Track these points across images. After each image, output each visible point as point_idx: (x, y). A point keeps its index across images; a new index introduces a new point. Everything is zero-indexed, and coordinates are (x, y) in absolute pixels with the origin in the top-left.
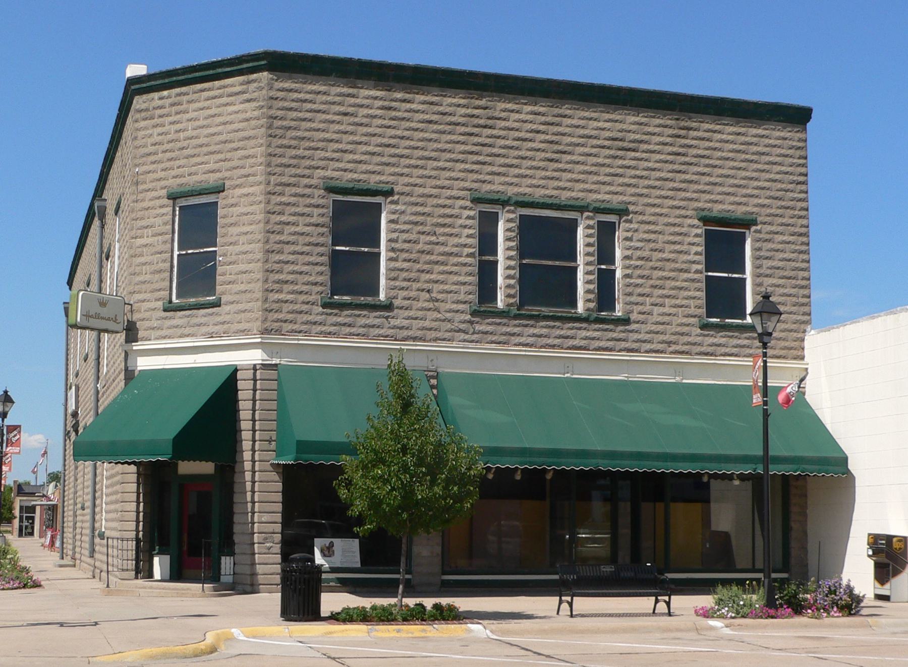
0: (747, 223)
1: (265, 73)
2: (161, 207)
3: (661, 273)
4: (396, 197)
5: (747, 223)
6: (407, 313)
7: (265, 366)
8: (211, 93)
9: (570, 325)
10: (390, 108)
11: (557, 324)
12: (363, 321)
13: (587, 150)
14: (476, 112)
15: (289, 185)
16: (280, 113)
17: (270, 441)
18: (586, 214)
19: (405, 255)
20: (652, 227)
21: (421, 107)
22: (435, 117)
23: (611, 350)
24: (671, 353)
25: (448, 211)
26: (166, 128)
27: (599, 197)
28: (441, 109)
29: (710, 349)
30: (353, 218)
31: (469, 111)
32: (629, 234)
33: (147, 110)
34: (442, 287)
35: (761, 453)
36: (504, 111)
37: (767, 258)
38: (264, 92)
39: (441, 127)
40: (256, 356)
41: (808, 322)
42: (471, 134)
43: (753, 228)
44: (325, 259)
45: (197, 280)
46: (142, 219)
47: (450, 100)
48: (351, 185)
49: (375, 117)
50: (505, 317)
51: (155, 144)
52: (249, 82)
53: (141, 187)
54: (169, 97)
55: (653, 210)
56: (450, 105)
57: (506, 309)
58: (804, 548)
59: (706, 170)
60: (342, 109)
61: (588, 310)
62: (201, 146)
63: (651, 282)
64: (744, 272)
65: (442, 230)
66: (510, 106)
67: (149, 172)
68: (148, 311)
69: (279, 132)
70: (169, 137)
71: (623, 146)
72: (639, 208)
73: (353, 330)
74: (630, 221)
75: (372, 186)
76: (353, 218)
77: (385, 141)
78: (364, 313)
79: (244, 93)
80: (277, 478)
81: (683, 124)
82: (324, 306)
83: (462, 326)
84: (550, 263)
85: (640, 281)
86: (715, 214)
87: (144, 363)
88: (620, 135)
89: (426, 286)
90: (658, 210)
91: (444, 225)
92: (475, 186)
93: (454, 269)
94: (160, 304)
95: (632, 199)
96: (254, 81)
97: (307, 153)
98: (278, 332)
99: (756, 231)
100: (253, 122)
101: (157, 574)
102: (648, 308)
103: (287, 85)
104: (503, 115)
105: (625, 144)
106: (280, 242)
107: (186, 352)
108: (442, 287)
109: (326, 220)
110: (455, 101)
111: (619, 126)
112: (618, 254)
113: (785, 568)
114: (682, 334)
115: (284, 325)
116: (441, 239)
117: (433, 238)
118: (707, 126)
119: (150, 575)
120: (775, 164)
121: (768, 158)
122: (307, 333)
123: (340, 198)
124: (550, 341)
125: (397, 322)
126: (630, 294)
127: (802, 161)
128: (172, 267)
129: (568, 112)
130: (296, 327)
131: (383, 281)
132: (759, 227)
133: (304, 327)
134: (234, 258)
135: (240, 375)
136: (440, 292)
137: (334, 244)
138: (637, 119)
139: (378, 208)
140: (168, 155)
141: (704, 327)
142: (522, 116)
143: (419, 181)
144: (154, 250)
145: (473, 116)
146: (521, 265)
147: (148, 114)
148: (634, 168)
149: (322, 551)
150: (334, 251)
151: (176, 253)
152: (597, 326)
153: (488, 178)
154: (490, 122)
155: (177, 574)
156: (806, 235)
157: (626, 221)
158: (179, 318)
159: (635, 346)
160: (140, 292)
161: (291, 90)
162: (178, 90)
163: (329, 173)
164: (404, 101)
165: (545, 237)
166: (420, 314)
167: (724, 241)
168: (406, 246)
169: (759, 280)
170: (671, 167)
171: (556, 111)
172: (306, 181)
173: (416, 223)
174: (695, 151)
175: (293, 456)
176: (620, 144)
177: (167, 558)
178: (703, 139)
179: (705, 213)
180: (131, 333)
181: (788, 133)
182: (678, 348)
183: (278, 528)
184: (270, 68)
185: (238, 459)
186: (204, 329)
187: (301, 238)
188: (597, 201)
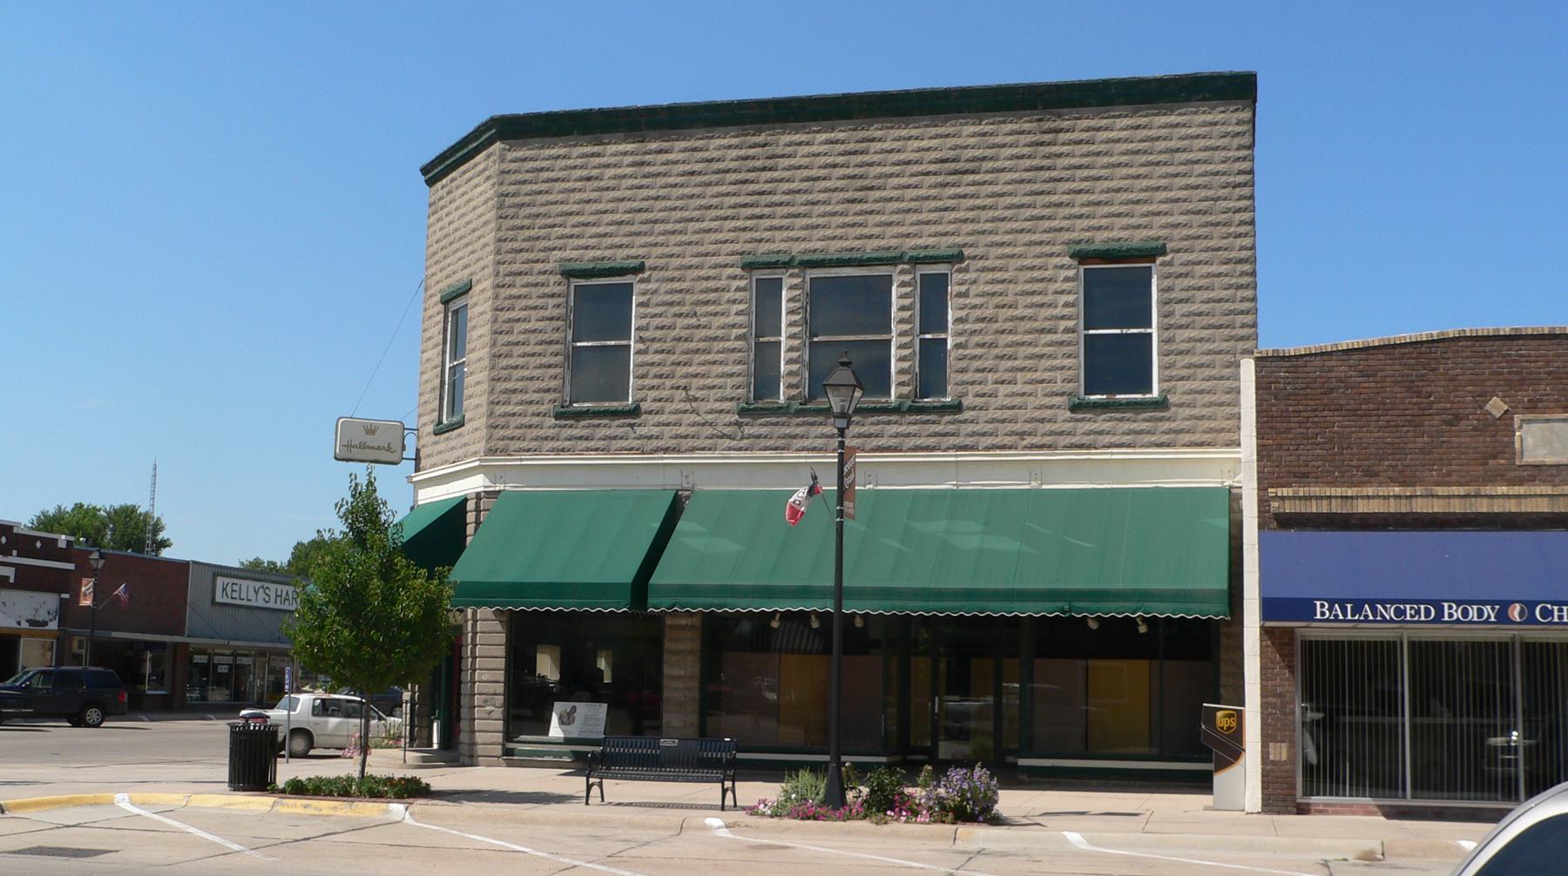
12: (603, 432)
35: (831, 583)
43: (1159, 260)
71: (956, 168)
94: (430, 428)
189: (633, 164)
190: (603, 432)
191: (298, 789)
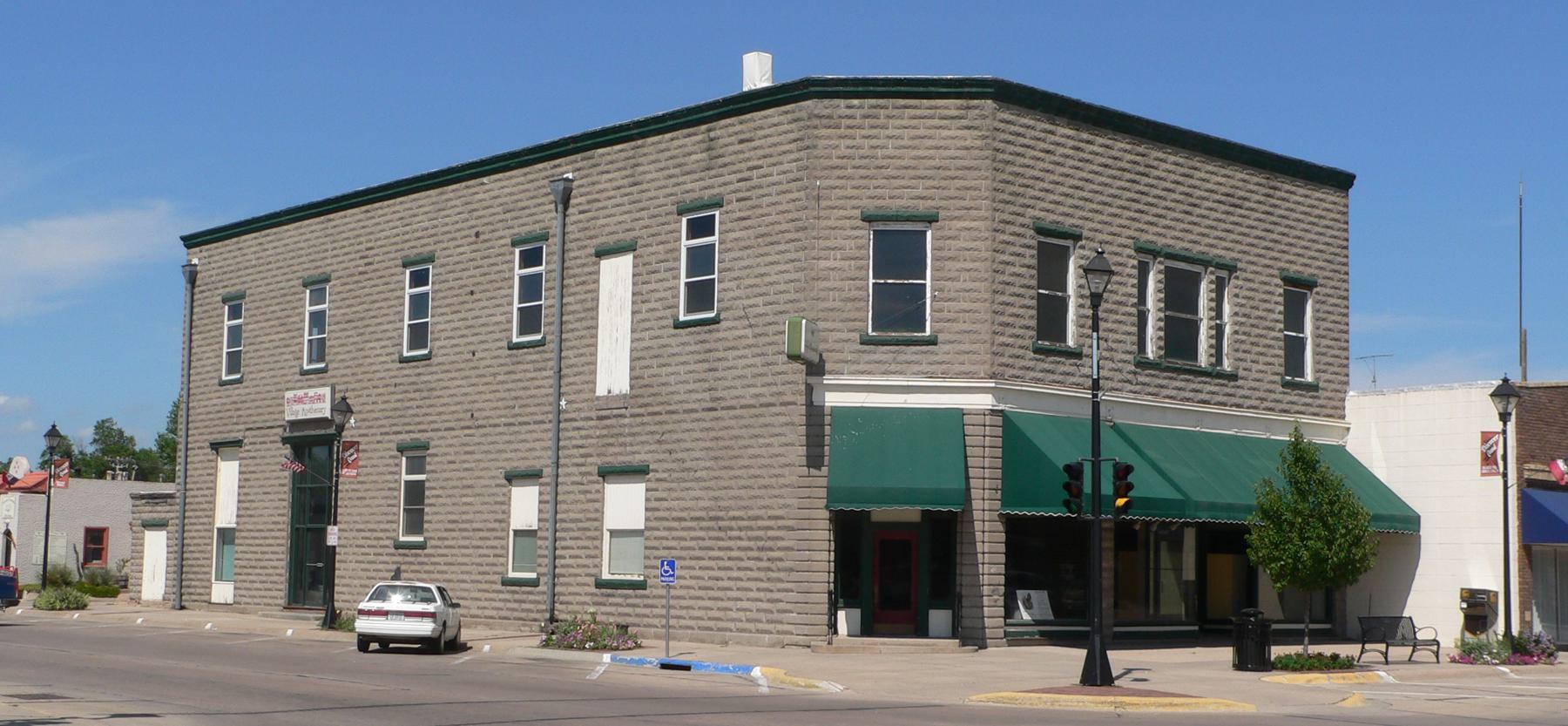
2: (853, 228)
7: (993, 412)
8: (918, 112)
10: (1078, 149)
12: (1062, 369)
16: (1001, 146)
22: (1110, 162)
26: (858, 141)
31: (1133, 157)
38: (988, 121)
40: (985, 401)
44: (1034, 303)
45: (899, 316)
46: (827, 238)
48: (1053, 227)
52: (968, 108)
53: (824, 203)
66: (1160, 155)
68: (839, 339)
70: (862, 152)
71: (1235, 203)
75: (1066, 229)
81: (1272, 183)
83: (1130, 377)
87: (832, 399)
88: (1231, 191)
92: (1136, 234)
94: (856, 336)
95: (1239, 256)
96: (976, 107)
98: (1002, 376)
134: (953, 295)
140: (862, 172)
147: (832, 122)
154: (1147, 170)
155: (868, 628)
158: (882, 353)
160: (825, 320)
162: (873, 101)
163: (1037, 213)
164: (1088, 142)
177: (857, 613)
180: (816, 369)
181: (1330, 197)
186: (916, 368)
189: (1074, 148)
190: (1062, 369)
191: (1286, 665)
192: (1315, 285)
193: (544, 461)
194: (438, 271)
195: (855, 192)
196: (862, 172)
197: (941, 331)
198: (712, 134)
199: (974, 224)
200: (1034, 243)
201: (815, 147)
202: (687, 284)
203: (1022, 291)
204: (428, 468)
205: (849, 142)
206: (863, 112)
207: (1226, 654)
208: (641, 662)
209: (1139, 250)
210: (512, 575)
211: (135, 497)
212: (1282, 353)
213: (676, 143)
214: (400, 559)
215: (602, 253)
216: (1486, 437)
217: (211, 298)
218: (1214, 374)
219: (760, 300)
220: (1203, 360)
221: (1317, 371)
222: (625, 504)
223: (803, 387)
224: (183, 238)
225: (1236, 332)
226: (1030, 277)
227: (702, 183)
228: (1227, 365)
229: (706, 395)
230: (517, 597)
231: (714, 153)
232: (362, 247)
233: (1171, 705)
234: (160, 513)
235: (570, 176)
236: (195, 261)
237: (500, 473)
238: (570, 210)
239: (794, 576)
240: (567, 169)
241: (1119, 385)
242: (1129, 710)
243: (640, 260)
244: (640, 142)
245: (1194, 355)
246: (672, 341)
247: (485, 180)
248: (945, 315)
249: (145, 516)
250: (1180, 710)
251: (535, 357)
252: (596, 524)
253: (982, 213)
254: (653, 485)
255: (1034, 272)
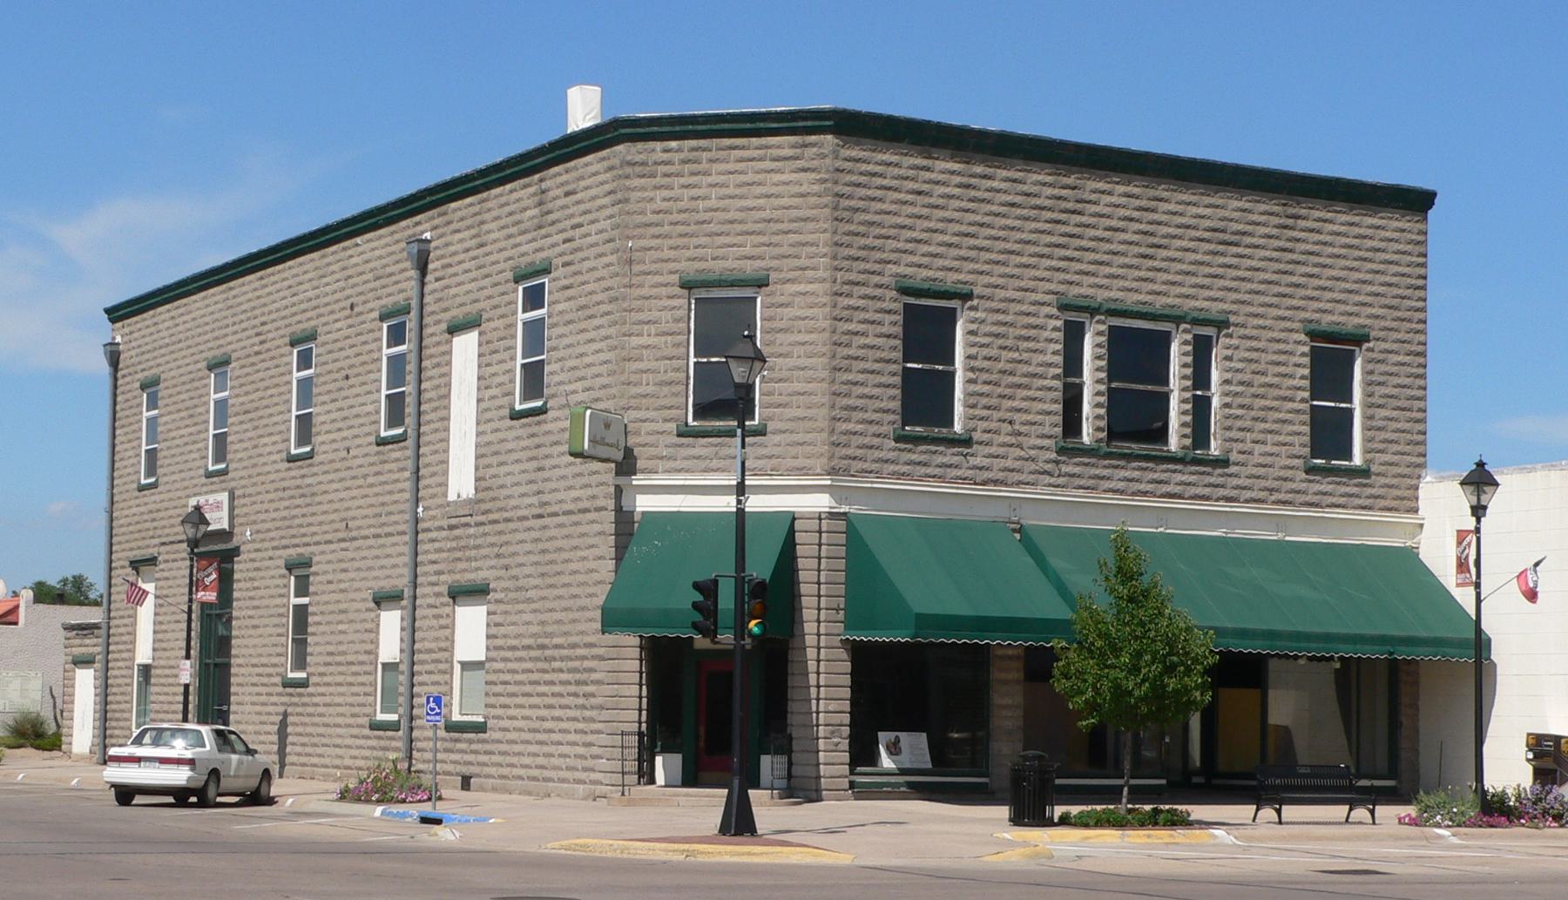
0: (1359, 339)
1: (829, 137)
2: (670, 297)
3: (1263, 402)
4: (975, 302)
5: (1359, 339)
6: (988, 450)
7: (832, 516)
9: (1164, 467)
10: (968, 186)
11: (1150, 465)
12: (940, 459)
13: (1185, 244)
14: (1064, 192)
15: (857, 284)
16: (847, 190)
17: (837, 610)
18: (1183, 326)
19: (985, 376)
20: (1254, 344)
21: (1003, 185)
22: (1018, 199)
23: (1208, 499)
24: (1274, 503)
25: (1032, 320)
26: (677, 192)
27: (1197, 304)
28: (1025, 188)
29: (1316, 499)
30: (926, 327)
31: (1056, 192)
32: (1229, 352)
33: (644, 164)
34: (1025, 417)
36: (1094, 191)
37: (1379, 384)
38: (827, 161)
39: (1025, 212)
40: (821, 502)
41: (1422, 466)
42: (1058, 222)
43: (1366, 346)
44: (897, 380)
45: (725, 404)
46: (640, 310)
47: (1035, 177)
48: (926, 286)
49: (952, 197)
50: (1093, 456)
51: (659, 212)
53: (637, 268)
54: (679, 150)
55: (1256, 322)
56: (1035, 183)
57: (1095, 445)
58: (1415, 751)
59: (1316, 270)
60: (916, 186)
61: (1184, 448)
62: (731, 222)
63: (1253, 413)
64: (1350, 401)
65: (1026, 344)
66: (1101, 185)
67: (650, 249)
69: (846, 214)
70: (681, 205)
71: (1225, 239)
72: (1240, 319)
73: (929, 471)
74: (1230, 336)
76: (926, 327)
77: (964, 228)
78: (941, 448)
79: (797, 158)
80: (845, 656)
81: (1291, 211)
82: (897, 440)
83: (1048, 467)
84: (1141, 387)
85: (1240, 412)
86: (1324, 327)
87: (645, 504)
88: (1221, 225)
89: (1008, 415)
90: (1261, 322)
91: (1028, 339)
92: (1062, 288)
93: (1039, 394)
94: (672, 426)
95: (1234, 307)
97: (878, 242)
98: (846, 472)
99: (1369, 350)
100: (813, 200)
101: (660, 776)
102: (1248, 446)
103: (854, 153)
104: (1093, 197)
105: (1226, 237)
106: (848, 357)
107: (685, 490)
108: (1025, 417)
109: (898, 330)
110: (1040, 178)
111: (1221, 213)
112: (1215, 376)
113: (1393, 773)
114: (1285, 479)
115: (854, 463)
116: (1025, 356)
117: (1016, 355)
118: (1317, 214)
119: (652, 781)
120: (1391, 263)
121: (1383, 256)
122: (878, 474)
123: (912, 301)
124: (1142, 487)
125: (978, 461)
126: (1229, 428)
127: (1421, 260)
128: (688, 378)
129: (1165, 194)
130: (866, 466)
131: (959, 409)
132: (1371, 345)
133: (874, 466)
134: (785, 374)
135: (798, 525)
136: (1023, 424)
137: (906, 360)
138: (1240, 204)
139: (950, 317)
140: (681, 229)
141: (1311, 470)
142: (1114, 199)
143: (1001, 281)
144: (659, 354)
145: (1059, 198)
146: (1109, 389)
148: (1236, 267)
149: (888, 748)
150: (905, 369)
151: (692, 360)
152: (1193, 468)
153: (1076, 278)
154: (1079, 206)
156: (1423, 354)
157: (1227, 336)
158: (702, 447)
159: (1234, 493)
160: (637, 408)
161: (858, 160)
162: (693, 143)
163: (901, 270)
164: (985, 177)
165: (1137, 354)
166: (1001, 451)
167: (1331, 359)
168: (986, 364)
169: (1370, 412)
170: (1277, 266)
171: (1151, 193)
172: (876, 279)
173: (997, 336)
174: (1304, 247)
175: (911, 631)
176: (1221, 236)
177: (677, 759)
178: (1312, 231)
179: (1313, 326)
180: (627, 465)
181: (1393, 224)
182: (1281, 496)
183: (846, 719)
184: (836, 131)
185: (797, 632)
187: (870, 353)
188: (1196, 309)
189: (960, 186)
190: (940, 459)
191: (1065, 821)
192: (1366, 339)
193: (403, 582)
194: (321, 350)
195: (672, 254)
196: (681, 229)
197: (771, 419)
198: (544, 186)
199: (810, 288)
200: (898, 306)
201: (627, 201)
202: (523, 366)
203: (877, 366)
204: (312, 589)
205: (666, 193)
206: (682, 156)
207: (1003, 812)
208: (404, 815)
209: (1064, 307)
210: (381, 717)
211: (69, 628)
212: (1306, 429)
213: (515, 196)
214: (285, 699)
215: (454, 329)
216: (1461, 536)
217: (130, 384)
218: (1196, 457)
219: (579, 385)
220: (1174, 443)
221: (1366, 451)
222: (470, 630)
223: (612, 489)
224: (107, 311)
225: (1227, 405)
226: (893, 349)
227: (535, 245)
228: (1215, 449)
229: (534, 500)
230: (382, 743)
231: (545, 208)
232: (257, 322)
233: (749, 854)
234: (92, 646)
235: (428, 235)
236: (118, 339)
237: (368, 595)
238: (429, 278)
239: (606, 715)
240: (424, 226)
241: (1031, 478)
242: (700, 859)
243: (485, 338)
244: (485, 195)
245: (1161, 435)
246: (511, 435)
247: (358, 240)
248: (776, 399)
249: (77, 651)
250: (756, 860)
251: (397, 455)
252: (446, 654)
253: (820, 274)
254: (493, 607)
255: (898, 342)
